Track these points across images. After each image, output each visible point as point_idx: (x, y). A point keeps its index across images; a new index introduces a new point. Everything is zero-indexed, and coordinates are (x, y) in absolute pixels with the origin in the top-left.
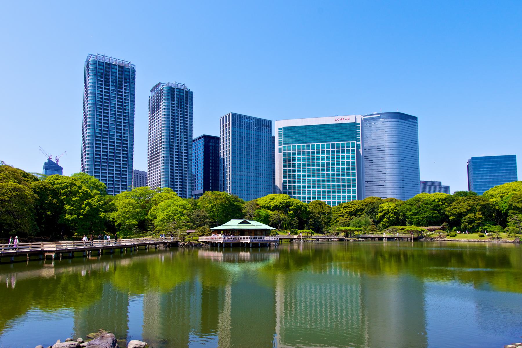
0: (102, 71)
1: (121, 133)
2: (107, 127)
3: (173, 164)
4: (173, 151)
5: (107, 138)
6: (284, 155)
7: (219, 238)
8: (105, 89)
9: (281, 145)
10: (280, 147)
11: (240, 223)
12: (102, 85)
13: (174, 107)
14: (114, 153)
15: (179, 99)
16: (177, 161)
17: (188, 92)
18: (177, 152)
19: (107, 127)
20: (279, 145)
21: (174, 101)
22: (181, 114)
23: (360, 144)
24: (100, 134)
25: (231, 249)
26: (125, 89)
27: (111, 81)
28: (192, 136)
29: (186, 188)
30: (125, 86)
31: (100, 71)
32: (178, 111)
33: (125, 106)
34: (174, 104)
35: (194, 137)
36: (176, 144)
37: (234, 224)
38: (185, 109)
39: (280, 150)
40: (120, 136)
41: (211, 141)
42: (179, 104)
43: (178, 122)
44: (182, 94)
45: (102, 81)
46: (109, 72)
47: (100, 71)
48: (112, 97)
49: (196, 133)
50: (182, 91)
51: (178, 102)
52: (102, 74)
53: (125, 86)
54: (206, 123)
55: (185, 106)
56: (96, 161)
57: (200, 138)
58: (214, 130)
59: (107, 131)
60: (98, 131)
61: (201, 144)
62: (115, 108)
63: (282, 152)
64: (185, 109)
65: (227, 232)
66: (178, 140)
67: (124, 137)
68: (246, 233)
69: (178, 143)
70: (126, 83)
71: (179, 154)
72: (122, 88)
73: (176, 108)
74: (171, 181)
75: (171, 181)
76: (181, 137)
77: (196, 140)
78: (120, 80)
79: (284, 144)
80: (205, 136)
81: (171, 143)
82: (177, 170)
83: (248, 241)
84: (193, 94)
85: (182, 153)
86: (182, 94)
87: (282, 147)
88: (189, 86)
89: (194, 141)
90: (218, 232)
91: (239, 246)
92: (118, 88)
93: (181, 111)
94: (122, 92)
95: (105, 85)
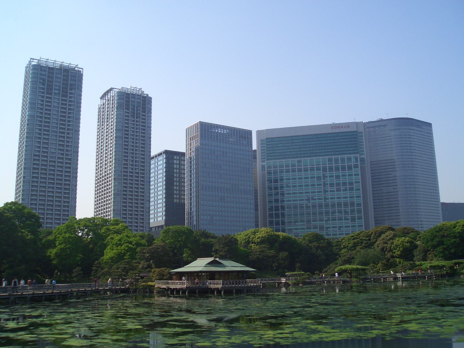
0: (44, 77)
1: (63, 150)
2: (47, 144)
3: (126, 214)
4: (127, 172)
5: (47, 157)
6: (268, 173)
7: (182, 284)
8: (47, 97)
9: (264, 161)
10: (263, 163)
11: (208, 264)
12: (43, 93)
13: (128, 116)
14: (54, 179)
15: (134, 107)
16: (132, 176)
17: (145, 97)
18: (132, 173)
19: (47, 144)
20: (262, 162)
21: (128, 109)
22: (136, 139)
23: (364, 158)
24: (39, 151)
25: (197, 295)
26: (70, 97)
27: (52, 92)
28: (150, 155)
29: (143, 200)
30: (71, 93)
31: (41, 77)
32: (134, 121)
33: (68, 134)
34: (128, 113)
35: (153, 154)
36: (130, 162)
37: (200, 265)
38: (142, 119)
39: (263, 167)
40: (62, 154)
41: (175, 157)
42: (134, 113)
43: (133, 124)
44: (139, 100)
45: (43, 89)
46: (52, 78)
47: (41, 77)
48: (55, 107)
49: (156, 148)
50: (139, 97)
51: (134, 110)
52: (44, 80)
53: (71, 93)
54: (168, 134)
55: (143, 115)
56: (33, 173)
57: (160, 154)
58: (180, 145)
59: (47, 148)
60: (37, 131)
61: (161, 162)
62: (57, 124)
63: (266, 169)
64: (142, 119)
65: (191, 275)
66: (133, 157)
67: (67, 155)
68: (217, 276)
69: (133, 161)
70: (71, 89)
71: (134, 175)
72: (66, 96)
73: (131, 118)
74: (124, 202)
75: (124, 202)
76: (136, 157)
77: (156, 156)
78: (64, 86)
79: (268, 160)
80: (167, 152)
81: (124, 162)
82: (132, 180)
83: (220, 286)
84: (152, 100)
85: (138, 173)
86: (139, 100)
87: (265, 163)
88: (147, 91)
89: (153, 158)
90: (180, 275)
91: (206, 293)
92: (62, 96)
93: (137, 121)
94: (66, 100)
95: (47, 94)
